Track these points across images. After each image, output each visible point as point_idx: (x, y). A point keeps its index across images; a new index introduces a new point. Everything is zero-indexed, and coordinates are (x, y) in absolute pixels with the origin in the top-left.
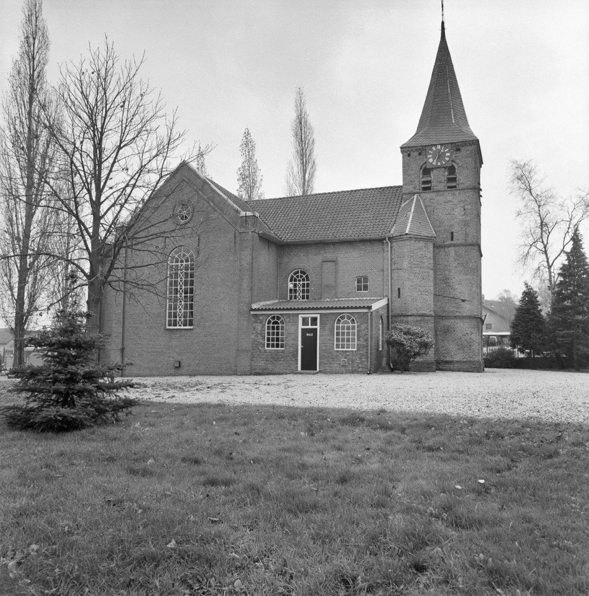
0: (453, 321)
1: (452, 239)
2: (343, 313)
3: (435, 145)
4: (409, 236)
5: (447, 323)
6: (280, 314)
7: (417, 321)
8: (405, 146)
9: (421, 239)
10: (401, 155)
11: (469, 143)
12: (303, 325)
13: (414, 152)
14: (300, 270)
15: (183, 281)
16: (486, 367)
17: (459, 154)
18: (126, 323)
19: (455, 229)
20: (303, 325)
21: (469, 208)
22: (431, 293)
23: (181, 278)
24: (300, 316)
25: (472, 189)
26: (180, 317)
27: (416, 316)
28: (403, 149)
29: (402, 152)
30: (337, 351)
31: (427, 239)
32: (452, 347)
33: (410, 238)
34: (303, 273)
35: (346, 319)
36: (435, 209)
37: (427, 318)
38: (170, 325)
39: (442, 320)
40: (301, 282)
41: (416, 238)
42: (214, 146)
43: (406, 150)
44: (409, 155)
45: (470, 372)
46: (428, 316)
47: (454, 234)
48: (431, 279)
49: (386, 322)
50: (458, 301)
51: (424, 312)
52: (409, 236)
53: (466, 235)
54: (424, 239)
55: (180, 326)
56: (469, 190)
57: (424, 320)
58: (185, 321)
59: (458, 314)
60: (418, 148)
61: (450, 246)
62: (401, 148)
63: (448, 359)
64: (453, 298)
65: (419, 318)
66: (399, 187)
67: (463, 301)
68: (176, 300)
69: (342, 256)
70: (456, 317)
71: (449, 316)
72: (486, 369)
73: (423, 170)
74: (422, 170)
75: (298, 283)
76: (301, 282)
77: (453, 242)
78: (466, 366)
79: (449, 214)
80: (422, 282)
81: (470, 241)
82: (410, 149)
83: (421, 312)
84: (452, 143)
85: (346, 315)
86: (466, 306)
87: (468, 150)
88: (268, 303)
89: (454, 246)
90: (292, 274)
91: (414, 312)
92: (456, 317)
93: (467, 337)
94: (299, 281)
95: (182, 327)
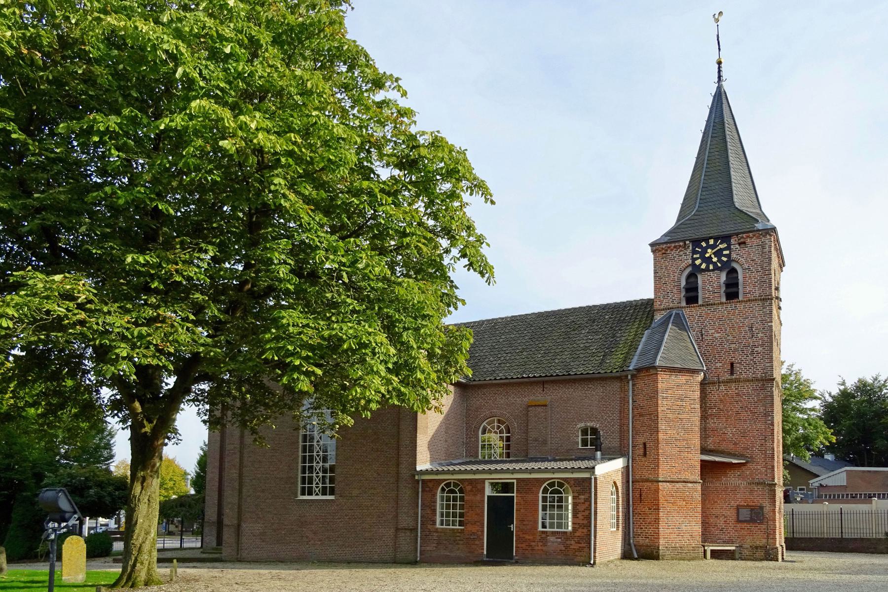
2: (552, 478)
6: (458, 480)
10: (652, 256)
12: (701, 453)
14: (496, 418)
15: (314, 483)
18: (244, 490)
20: (701, 453)
23: (318, 456)
24: (487, 483)
26: (317, 473)
28: (655, 247)
29: (653, 251)
30: (543, 532)
38: (303, 494)
49: (187, 556)
55: (317, 494)
58: (324, 489)
66: (649, 300)
68: (311, 460)
85: (556, 480)
90: (484, 423)
95: (320, 497)
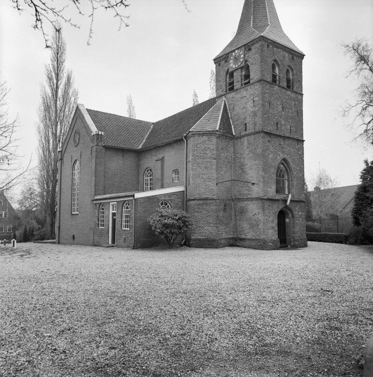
0: (246, 202)
1: (246, 130)
3: (234, 51)
4: (192, 133)
5: (242, 204)
7: (200, 204)
8: (216, 57)
9: (203, 134)
10: (215, 65)
11: (257, 41)
13: (222, 61)
16: (309, 240)
17: (250, 54)
19: (248, 120)
21: (257, 99)
22: (214, 180)
24: (111, 203)
25: (258, 82)
27: (198, 200)
29: (215, 63)
30: (125, 230)
31: (209, 133)
32: (245, 226)
33: (193, 134)
34: (151, 170)
35: (164, 205)
36: (235, 106)
37: (209, 201)
39: (239, 201)
40: (150, 178)
41: (198, 134)
42: (8, 90)
43: (217, 61)
44: (219, 64)
45: (257, 249)
46: (210, 200)
47: (247, 125)
48: (214, 167)
50: (250, 185)
51: (207, 196)
52: (192, 133)
53: (255, 124)
54: (207, 134)
56: (257, 84)
57: (206, 203)
59: (249, 196)
60: (224, 57)
61: (244, 136)
62: (214, 60)
63: (243, 237)
64: (246, 182)
65: (201, 202)
67: (253, 184)
69: (166, 155)
70: (248, 199)
71: (243, 199)
72: (309, 243)
73: (229, 74)
74: (228, 75)
75: (148, 178)
76: (150, 178)
77: (247, 132)
78: (253, 244)
79: (244, 108)
80: (205, 171)
81: (257, 129)
82: (219, 59)
83: (204, 196)
84: (245, 45)
86: (255, 188)
87: (256, 48)
88: (122, 194)
89: (247, 136)
91: (197, 197)
92: (248, 199)
93: (256, 217)
94: (149, 177)
